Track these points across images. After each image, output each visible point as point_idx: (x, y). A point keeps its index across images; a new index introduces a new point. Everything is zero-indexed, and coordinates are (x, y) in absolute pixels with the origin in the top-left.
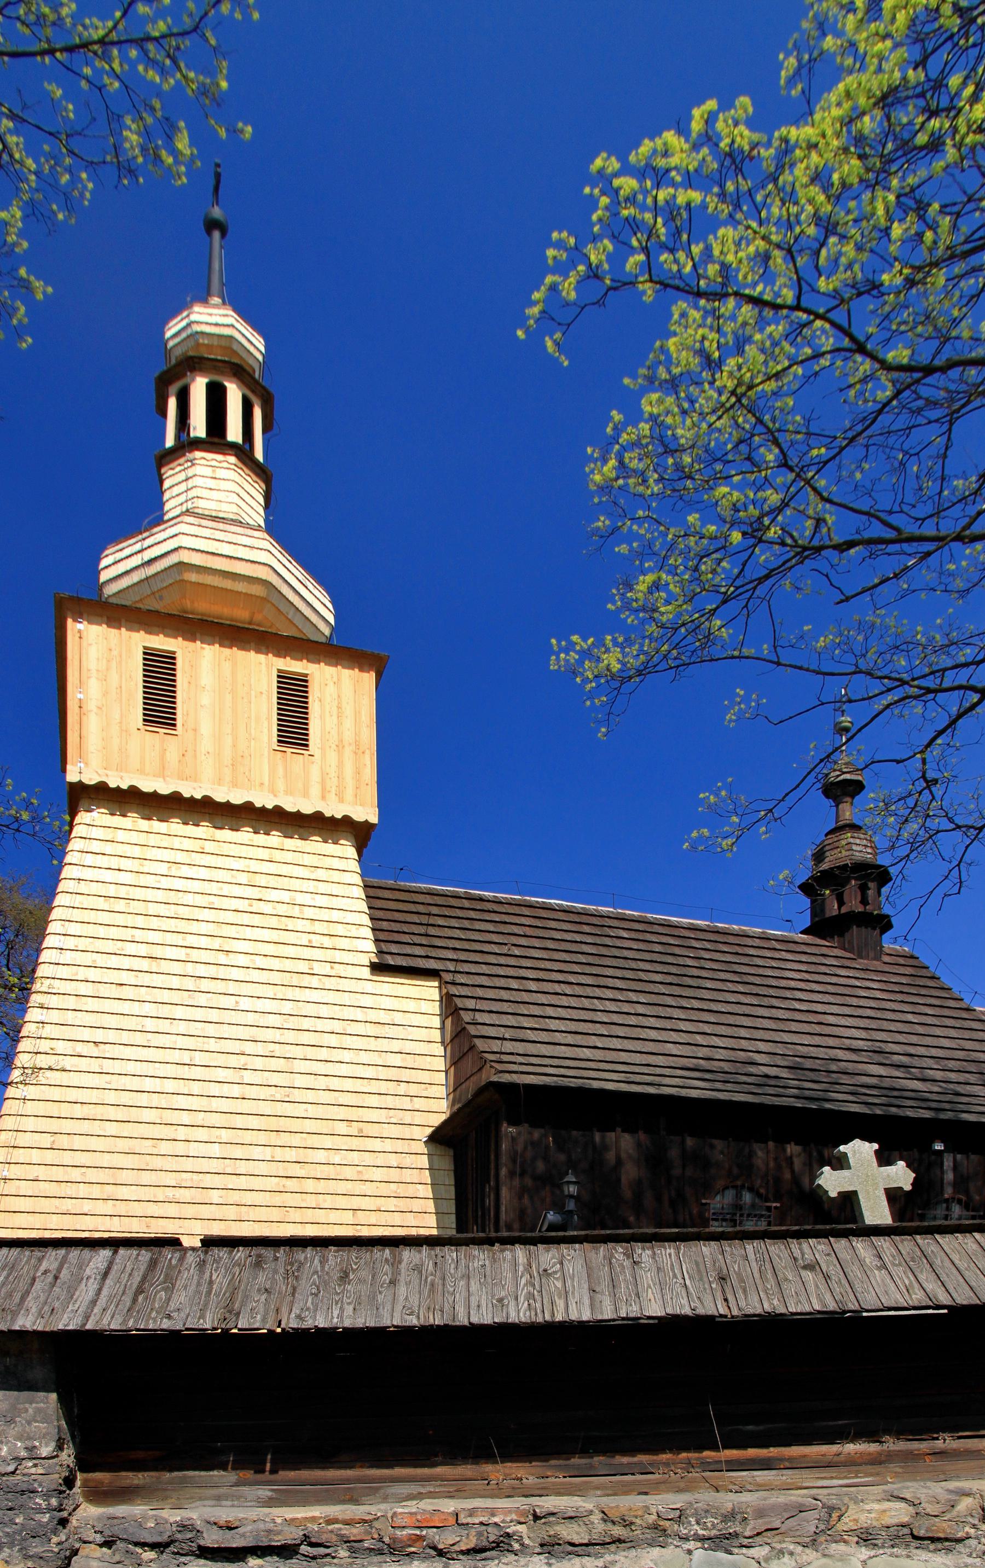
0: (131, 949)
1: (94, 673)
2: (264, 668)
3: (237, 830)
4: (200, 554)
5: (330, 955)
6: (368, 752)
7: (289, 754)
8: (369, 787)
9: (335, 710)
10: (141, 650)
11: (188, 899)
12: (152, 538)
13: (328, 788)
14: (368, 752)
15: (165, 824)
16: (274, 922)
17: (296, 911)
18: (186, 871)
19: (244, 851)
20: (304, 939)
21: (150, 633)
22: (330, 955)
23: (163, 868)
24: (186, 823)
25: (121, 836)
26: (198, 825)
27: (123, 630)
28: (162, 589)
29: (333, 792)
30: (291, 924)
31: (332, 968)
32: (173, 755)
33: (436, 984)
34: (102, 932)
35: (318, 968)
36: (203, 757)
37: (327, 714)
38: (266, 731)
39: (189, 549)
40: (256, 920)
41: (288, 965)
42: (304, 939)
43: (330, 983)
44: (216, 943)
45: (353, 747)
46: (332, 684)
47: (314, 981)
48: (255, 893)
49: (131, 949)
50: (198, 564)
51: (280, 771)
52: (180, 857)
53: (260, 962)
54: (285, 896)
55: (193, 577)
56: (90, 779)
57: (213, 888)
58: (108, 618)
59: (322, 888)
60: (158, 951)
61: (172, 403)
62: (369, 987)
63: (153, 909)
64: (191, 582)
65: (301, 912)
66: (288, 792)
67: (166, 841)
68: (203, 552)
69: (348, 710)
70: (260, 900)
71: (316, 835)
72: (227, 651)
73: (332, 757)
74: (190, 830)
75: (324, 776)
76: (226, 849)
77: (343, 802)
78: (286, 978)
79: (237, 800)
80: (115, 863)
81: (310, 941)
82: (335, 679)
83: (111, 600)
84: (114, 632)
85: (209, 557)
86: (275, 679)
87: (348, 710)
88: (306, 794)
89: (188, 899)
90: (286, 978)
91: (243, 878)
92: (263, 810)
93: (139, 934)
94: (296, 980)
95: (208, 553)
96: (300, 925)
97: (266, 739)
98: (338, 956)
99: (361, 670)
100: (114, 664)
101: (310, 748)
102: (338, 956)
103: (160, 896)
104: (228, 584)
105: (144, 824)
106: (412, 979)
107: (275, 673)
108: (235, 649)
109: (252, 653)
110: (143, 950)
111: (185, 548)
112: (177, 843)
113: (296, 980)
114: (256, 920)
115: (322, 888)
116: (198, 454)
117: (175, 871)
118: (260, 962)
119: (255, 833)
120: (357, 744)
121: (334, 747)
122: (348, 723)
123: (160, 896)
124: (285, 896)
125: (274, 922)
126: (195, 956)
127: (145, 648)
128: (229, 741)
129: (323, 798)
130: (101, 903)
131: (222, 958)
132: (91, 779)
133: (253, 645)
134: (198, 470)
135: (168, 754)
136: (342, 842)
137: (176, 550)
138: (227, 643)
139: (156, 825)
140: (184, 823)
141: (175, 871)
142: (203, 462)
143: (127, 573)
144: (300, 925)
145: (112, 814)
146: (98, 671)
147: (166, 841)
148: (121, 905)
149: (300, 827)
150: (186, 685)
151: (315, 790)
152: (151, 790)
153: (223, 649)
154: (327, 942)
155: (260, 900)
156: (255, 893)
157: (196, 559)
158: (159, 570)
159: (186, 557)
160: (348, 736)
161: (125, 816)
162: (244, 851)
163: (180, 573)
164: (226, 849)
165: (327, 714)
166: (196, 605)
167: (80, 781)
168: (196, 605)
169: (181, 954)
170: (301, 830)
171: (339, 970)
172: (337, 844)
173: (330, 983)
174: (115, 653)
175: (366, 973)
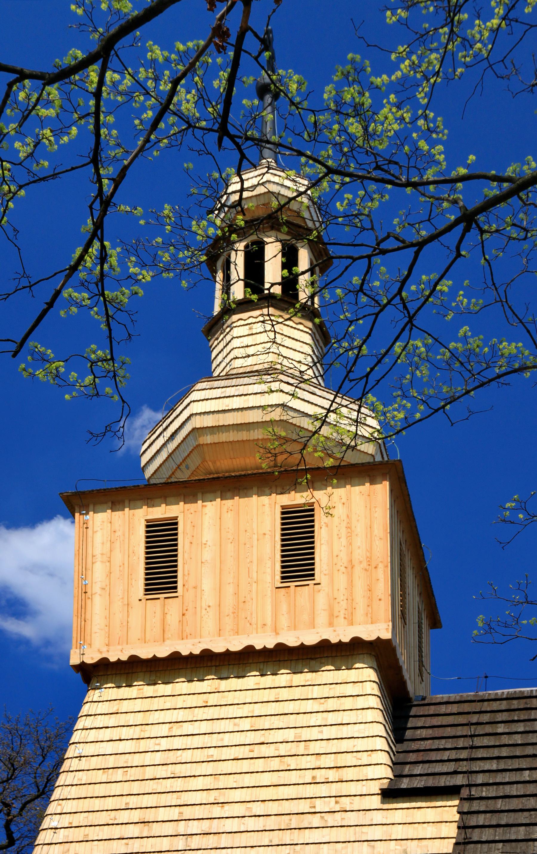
0: (124, 817)
1: (99, 558)
2: (267, 509)
3: (244, 677)
4: (211, 416)
5: (334, 789)
6: (381, 566)
7: (292, 588)
8: (382, 602)
9: (344, 531)
10: (143, 524)
11: (187, 756)
12: (174, 413)
13: (336, 614)
14: (381, 566)
15: (171, 685)
16: (275, 764)
17: (301, 748)
18: (188, 728)
19: (249, 697)
20: (308, 776)
21: (153, 506)
22: (334, 789)
23: (164, 730)
24: (338, 669)
25: (125, 706)
26: (203, 680)
27: (127, 510)
28: (186, 458)
29: (342, 616)
30: (293, 763)
31: (337, 802)
32: (173, 618)
33: (457, 802)
34: (97, 804)
35: (320, 805)
36: (204, 612)
37: (335, 537)
38: (269, 571)
39: (200, 414)
40: (259, 765)
41: (287, 807)
42: (308, 776)
43: (337, 819)
44: (211, 797)
45: (365, 564)
46: (341, 505)
47: (316, 820)
48: (258, 737)
49: (124, 817)
50: (210, 425)
51: (284, 608)
52: (180, 715)
53: (258, 808)
54: (290, 735)
55: (208, 439)
56: (91, 658)
57: (214, 740)
58: (113, 503)
59: (332, 718)
60: (150, 815)
61: (220, 276)
62: (378, 817)
63: (150, 772)
64: (207, 444)
65: (306, 748)
66: (294, 627)
67: (169, 703)
68: (214, 412)
69: (359, 528)
70: (263, 743)
71: (253, 671)
72: (229, 503)
73: (341, 581)
74: (197, 686)
75: (332, 600)
76: (230, 698)
77: (352, 624)
78: (283, 822)
79: (236, 646)
80: (115, 734)
81: (314, 778)
82: (344, 500)
83: (152, 482)
84: (118, 514)
85: (221, 415)
86: (278, 516)
87: (359, 528)
88: (312, 625)
89: (187, 756)
90: (283, 822)
91: (246, 724)
92: (265, 651)
93: (133, 801)
94: (295, 821)
95: (218, 412)
96: (305, 762)
97: (269, 578)
98: (345, 788)
99: (372, 483)
100: (117, 544)
101: (316, 576)
102: (345, 788)
103: (158, 758)
104: (243, 435)
105: (149, 690)
106: (431, 801)
107: (279, 510)
108: (237, 498)
109: (255, 497)
110: (136, 816)
111: (196, 414)
112: (180, 702)
113: (295, 821)
114: (259, 765)
115: (332, 718)
116: (235, 317)
117: (177, 730)
118: (258, 808)
119: (262, 675)
120: (369, 560)
121: (343, 569)
122: (359, 542)
123: (158, 758)
124: (290, 735)
125: (275, 764)
126: (188, 812)
127: (147, 521)
128: (229, 590)
129: (331, 624)
130: (101, 776)
131: (217, 811)
132: (92, 659)
133: (255, 489)
134: (236, 332)
135: (168, 617)
136: (357, 665)
137: (189, 418)
138: (229, 494)
139: (162, 689)
140: (188, 681)
141: (177, 730)
142: (241, 323)
143: (158, 452)
144: (305, 762)
145: (119, 687)
146: (102, 554)
147: (169, 703)
148: (119, 775)
149: (312, 659)
150: (187, 545)
151: (322, 618)
152: (150, 656)
153: (224, 502)
154: (332, 775)
155: (263, 743)
156: (258, 737)
157: (209, 421)
158: (180, 442)
159: (198, 422)
160: (359, 554)
161: (130, 686)
162: (249, 697)
163: (196, 439)
164: (230, 698)
165: (335, 537)
166: (218, 464)
167: (378, 638)
168: (218, 464)
169: (174, 813)
170: (313, 663)
171: (346, 803)
172: (351, 669)
173: (337, 819)
174: (118, 533)
175: (376, 801)
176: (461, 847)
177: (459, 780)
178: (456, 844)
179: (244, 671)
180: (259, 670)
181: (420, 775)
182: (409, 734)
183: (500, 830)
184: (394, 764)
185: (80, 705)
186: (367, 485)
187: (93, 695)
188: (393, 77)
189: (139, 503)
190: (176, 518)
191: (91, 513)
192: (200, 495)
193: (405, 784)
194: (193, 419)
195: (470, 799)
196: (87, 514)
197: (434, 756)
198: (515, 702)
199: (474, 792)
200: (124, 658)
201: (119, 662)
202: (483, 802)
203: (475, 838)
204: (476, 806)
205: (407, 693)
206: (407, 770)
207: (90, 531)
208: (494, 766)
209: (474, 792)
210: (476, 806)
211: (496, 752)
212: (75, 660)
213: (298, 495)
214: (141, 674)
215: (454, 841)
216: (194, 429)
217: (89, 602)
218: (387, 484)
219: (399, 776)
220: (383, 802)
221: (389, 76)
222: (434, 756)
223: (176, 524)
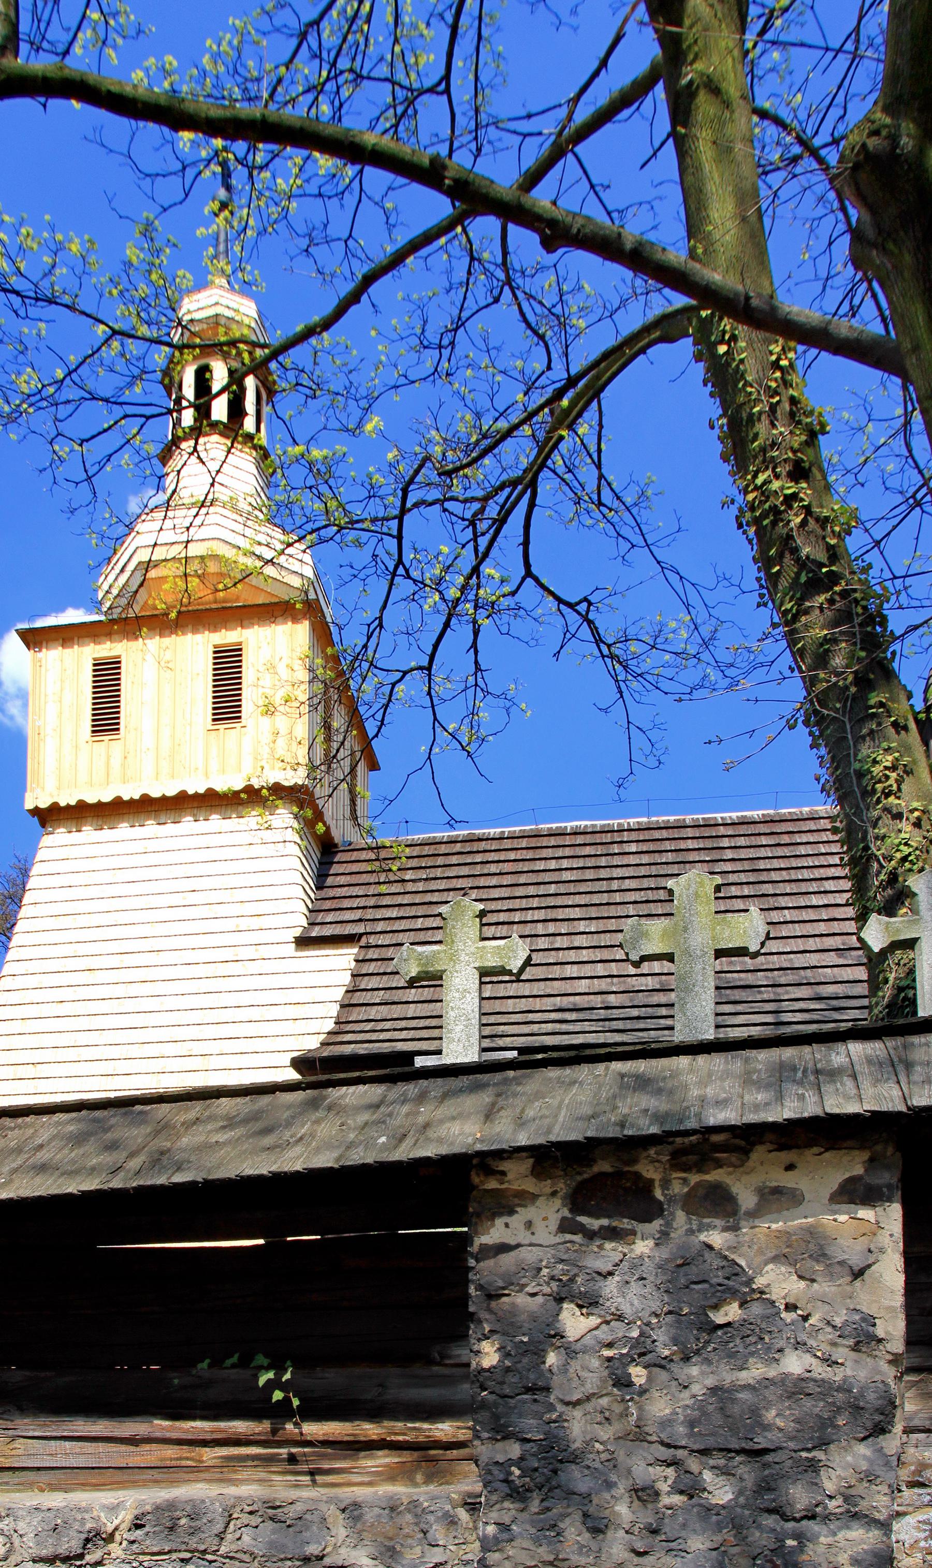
7: (222, 731)
27: (76, 647)
56: (44, 804)
84: (68, 651)
101: (242, 720)
109: (190, 635)
127: (95, 659)
176: (350, 995)
177: (360, 929)
178: (347, 992)
179: (180, 816)
180: (194, 815)
181: (331, 923)
182: (330, 881)
183: (385, 978)
184: (310, 911)
185: (34, 849)
186: (290, 623)
187: (46, 840)
188: (210, 231)
189: (87, 640)
190: (119, 657)
191: (44, 650)
192: (190, 627)
193: (315, 932)
194: (138, 551)
195: (368, 947)
196: (40, 651)
197: (346, 903)
198: (427, 848)
199: (372, 940)
200: (73, 803)
201: (68, 807)
202: (378, 950)
203: (362, 987)
204: (372, 954)
205: (333, 838)
206: (320, 918)
207: (43, 669)
208: (394, 913)
209: (372, 940)
210: (372, 954)
211: (400, 900)
212: (29, 805)
213: (229, 633)
214: (89, 819)
215: (345, 988)
216: (139, 563)
217: (42, 744)
218: (307, 623)
219: (312, 924)
220: (296, 950)
221: (207, 229)
222: (346, 903)
223: (119, 662)
